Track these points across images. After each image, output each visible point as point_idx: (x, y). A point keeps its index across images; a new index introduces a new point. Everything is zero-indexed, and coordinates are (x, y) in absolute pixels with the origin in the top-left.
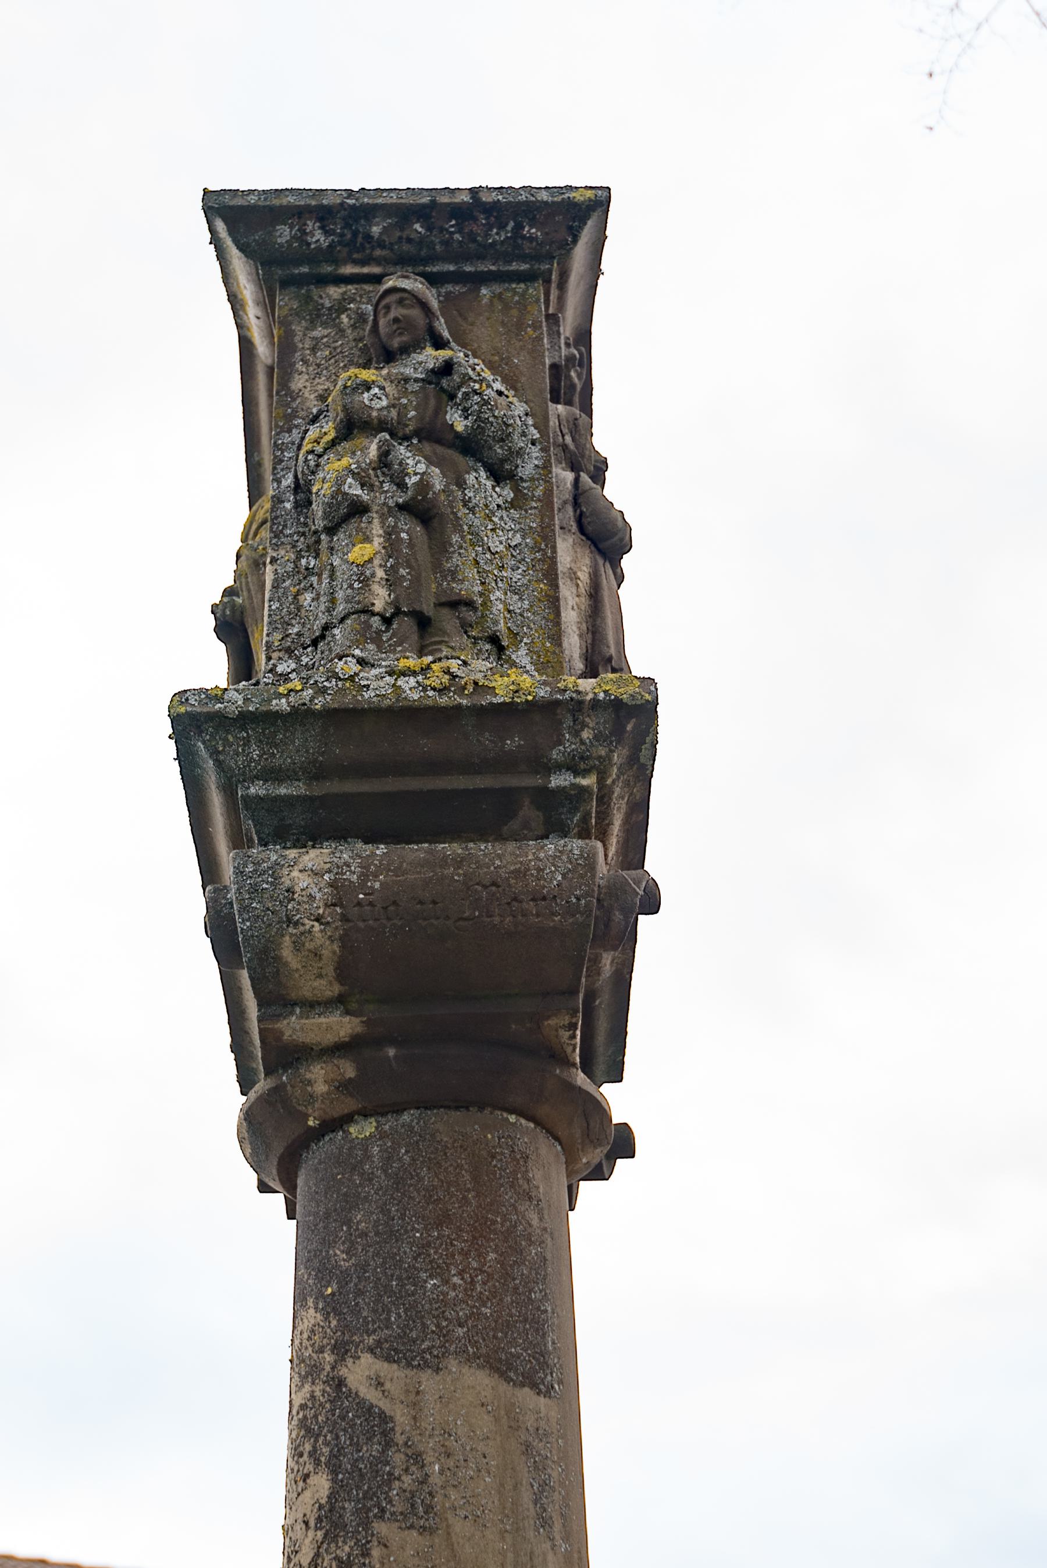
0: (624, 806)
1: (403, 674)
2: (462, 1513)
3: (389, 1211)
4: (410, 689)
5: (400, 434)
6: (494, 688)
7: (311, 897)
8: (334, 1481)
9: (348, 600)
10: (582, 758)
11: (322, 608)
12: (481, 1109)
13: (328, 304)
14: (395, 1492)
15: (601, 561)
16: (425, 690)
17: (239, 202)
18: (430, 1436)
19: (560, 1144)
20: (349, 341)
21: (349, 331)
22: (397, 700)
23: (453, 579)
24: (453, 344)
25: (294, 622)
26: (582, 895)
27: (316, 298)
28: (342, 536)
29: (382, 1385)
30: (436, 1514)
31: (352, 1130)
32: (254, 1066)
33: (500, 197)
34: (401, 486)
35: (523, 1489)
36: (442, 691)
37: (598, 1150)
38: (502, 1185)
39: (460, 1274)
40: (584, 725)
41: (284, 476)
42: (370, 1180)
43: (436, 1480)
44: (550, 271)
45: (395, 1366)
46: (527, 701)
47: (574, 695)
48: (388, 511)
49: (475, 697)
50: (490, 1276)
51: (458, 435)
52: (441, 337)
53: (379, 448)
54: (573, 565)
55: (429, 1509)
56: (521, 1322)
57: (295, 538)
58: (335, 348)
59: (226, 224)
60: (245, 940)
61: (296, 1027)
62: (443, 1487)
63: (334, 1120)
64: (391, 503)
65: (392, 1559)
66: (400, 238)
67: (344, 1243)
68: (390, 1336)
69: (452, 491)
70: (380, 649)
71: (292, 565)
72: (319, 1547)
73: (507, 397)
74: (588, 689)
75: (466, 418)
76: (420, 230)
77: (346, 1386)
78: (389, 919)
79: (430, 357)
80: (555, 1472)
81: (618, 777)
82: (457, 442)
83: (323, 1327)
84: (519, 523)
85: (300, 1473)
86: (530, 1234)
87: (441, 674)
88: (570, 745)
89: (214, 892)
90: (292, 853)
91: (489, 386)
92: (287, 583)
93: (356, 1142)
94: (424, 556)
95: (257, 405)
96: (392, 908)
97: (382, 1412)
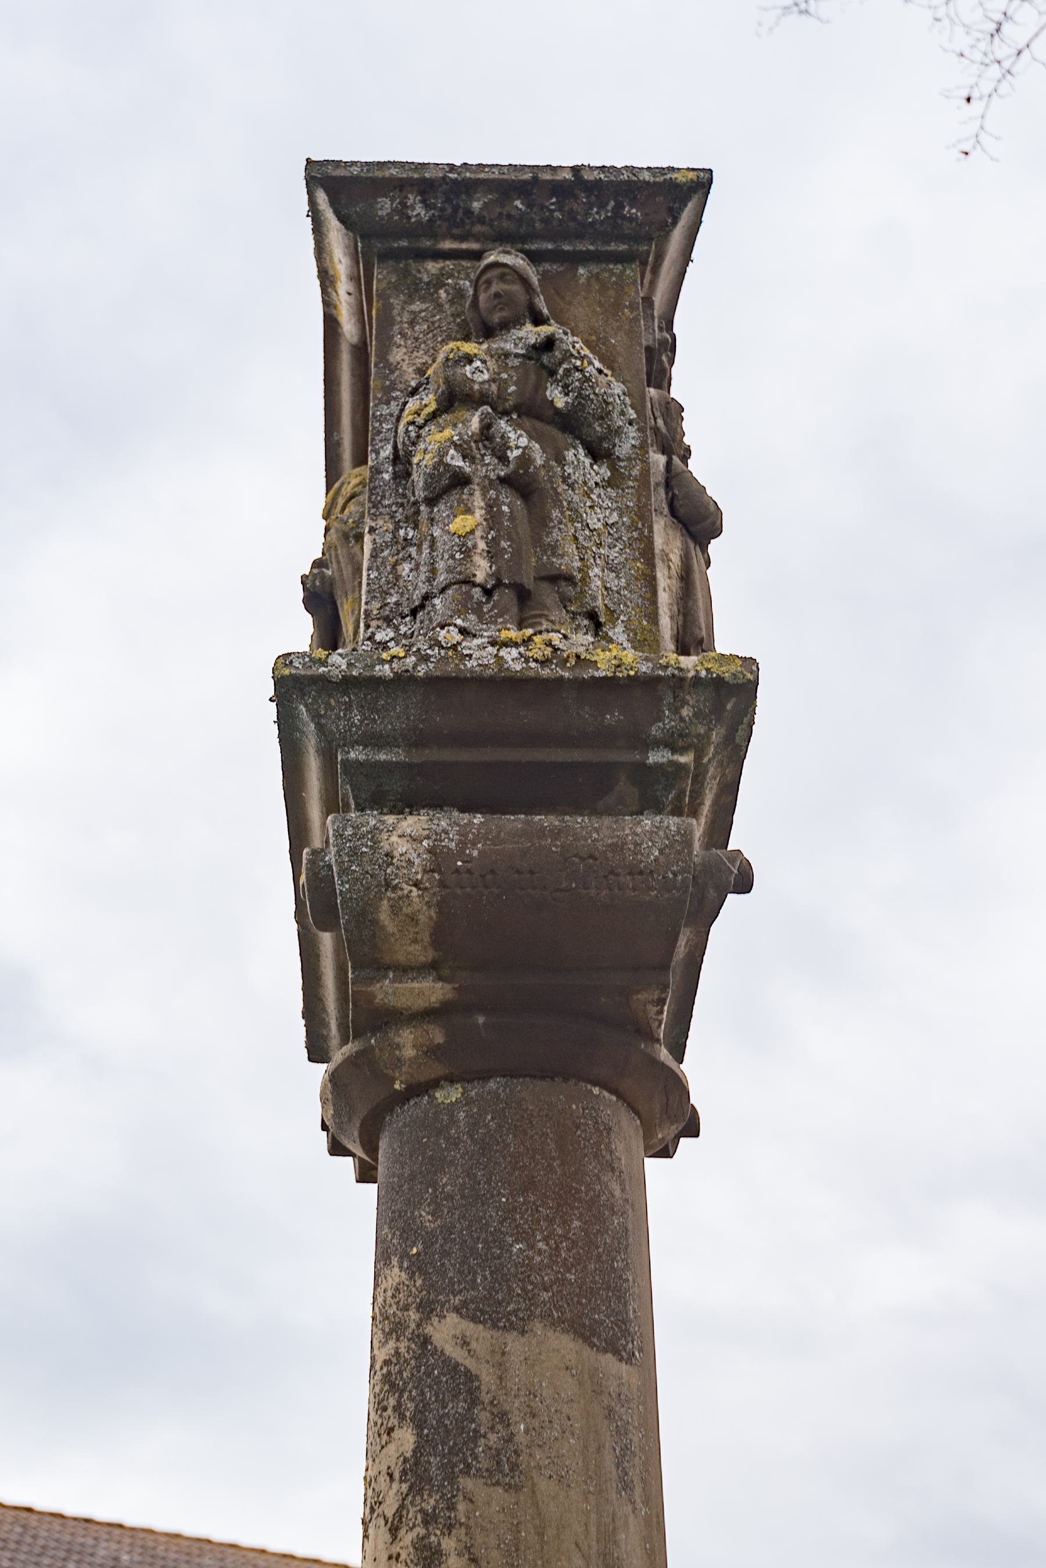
0: (715, 786)
1: (505, 644)
2: (548, 1473)
3: (475, 1175)
4: (513, 660)
5: (500, 409)
6: (596, 662)
7: (410, 863)
8: (419, 1435)
9: (449, 570)
10: (681, 735)
11: (423, 577)
12: (566, 1079)
13: (426, 279)
14: (481, 1449)
15: (692, 545)
16: (527, 661)
17: (341, 172)
18: (515, 1396)
19: (640, 1118)
20: (447, 316)
21: (447, 306)
22: (500, 670)
23: (553, 554)
24: (552, 321)
25: (392, 591)
26: (679, 872)
27: (414, 272)
28: (443, 507)
29: (468, 1344)
30: (521, 1472)
31: (438, 1095)
32: (325, 1032)
33: (602, 176)
34: (503, 459)
35: (606, 1452)
36: (544, 662)
37: (674, 1127)
38: (586, 1155)
39: (546, 1239)
40: (684, 703)
41: (382, 447)
42: (456, 1145)
43: (521, 1439)
44: (648, 253)
45: (481, 1327)
46: (629, 675)
47: (676, 672)
48: (488, 485)
49: (577, 670)
50: (575, 1243)
51: (557, 411)
52: (541, 313)
53: (481, 421)
54: (665, 547)
55: (514, 1467)
56: (604, 1289)
57: (394, 508)
58: (433, 323)
59: (328, 195)
60: (343, 902)
61: (388, 991)
62: (528, 1447)
63: (420, 1084)
64: (493, 476)
65: (477, 1514)
66: (501, 214)
67: (429, 1205)
68: (476, 1297)
69: (553, 467)
70: (481, 620)
71: (390, 535)
72: (404, 1500)
73: (606, 375)
74: (690, 667)
75: (567, 394)
76: (520, 206)
77: (431, 1344)
78: (486, 887)
79: (530, 333)
80: (636, 1437)
81: (714, 756)
82: (557, 418)
83: (408, 1286)
84: (617, 502)
85: (384, 1426)
86: (613, 1205)
87: (543, 646)
88: (669, 723)
89: (312, 854)
90: (390, 819)
91: (590, 363)
92: (386, 553)
93: (442, 1106)
94: (524, 530)
95: (339, 384)
96: (489, 877)
97: (468, 1371)
